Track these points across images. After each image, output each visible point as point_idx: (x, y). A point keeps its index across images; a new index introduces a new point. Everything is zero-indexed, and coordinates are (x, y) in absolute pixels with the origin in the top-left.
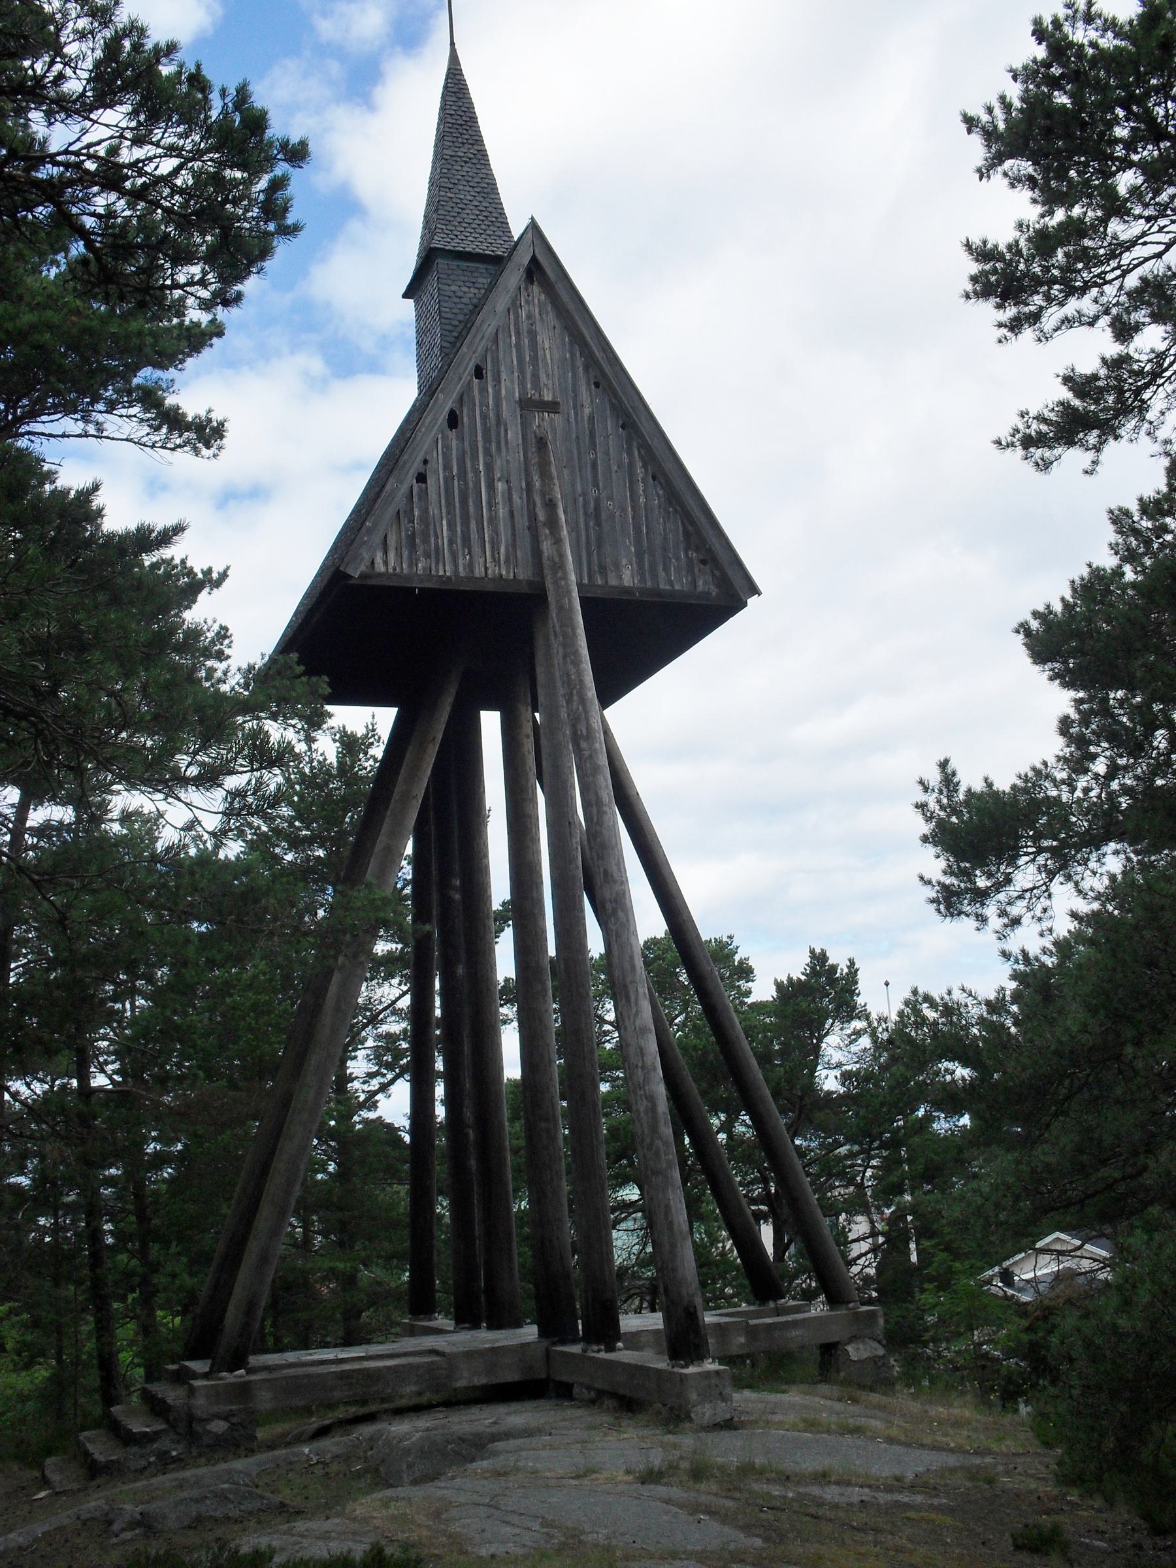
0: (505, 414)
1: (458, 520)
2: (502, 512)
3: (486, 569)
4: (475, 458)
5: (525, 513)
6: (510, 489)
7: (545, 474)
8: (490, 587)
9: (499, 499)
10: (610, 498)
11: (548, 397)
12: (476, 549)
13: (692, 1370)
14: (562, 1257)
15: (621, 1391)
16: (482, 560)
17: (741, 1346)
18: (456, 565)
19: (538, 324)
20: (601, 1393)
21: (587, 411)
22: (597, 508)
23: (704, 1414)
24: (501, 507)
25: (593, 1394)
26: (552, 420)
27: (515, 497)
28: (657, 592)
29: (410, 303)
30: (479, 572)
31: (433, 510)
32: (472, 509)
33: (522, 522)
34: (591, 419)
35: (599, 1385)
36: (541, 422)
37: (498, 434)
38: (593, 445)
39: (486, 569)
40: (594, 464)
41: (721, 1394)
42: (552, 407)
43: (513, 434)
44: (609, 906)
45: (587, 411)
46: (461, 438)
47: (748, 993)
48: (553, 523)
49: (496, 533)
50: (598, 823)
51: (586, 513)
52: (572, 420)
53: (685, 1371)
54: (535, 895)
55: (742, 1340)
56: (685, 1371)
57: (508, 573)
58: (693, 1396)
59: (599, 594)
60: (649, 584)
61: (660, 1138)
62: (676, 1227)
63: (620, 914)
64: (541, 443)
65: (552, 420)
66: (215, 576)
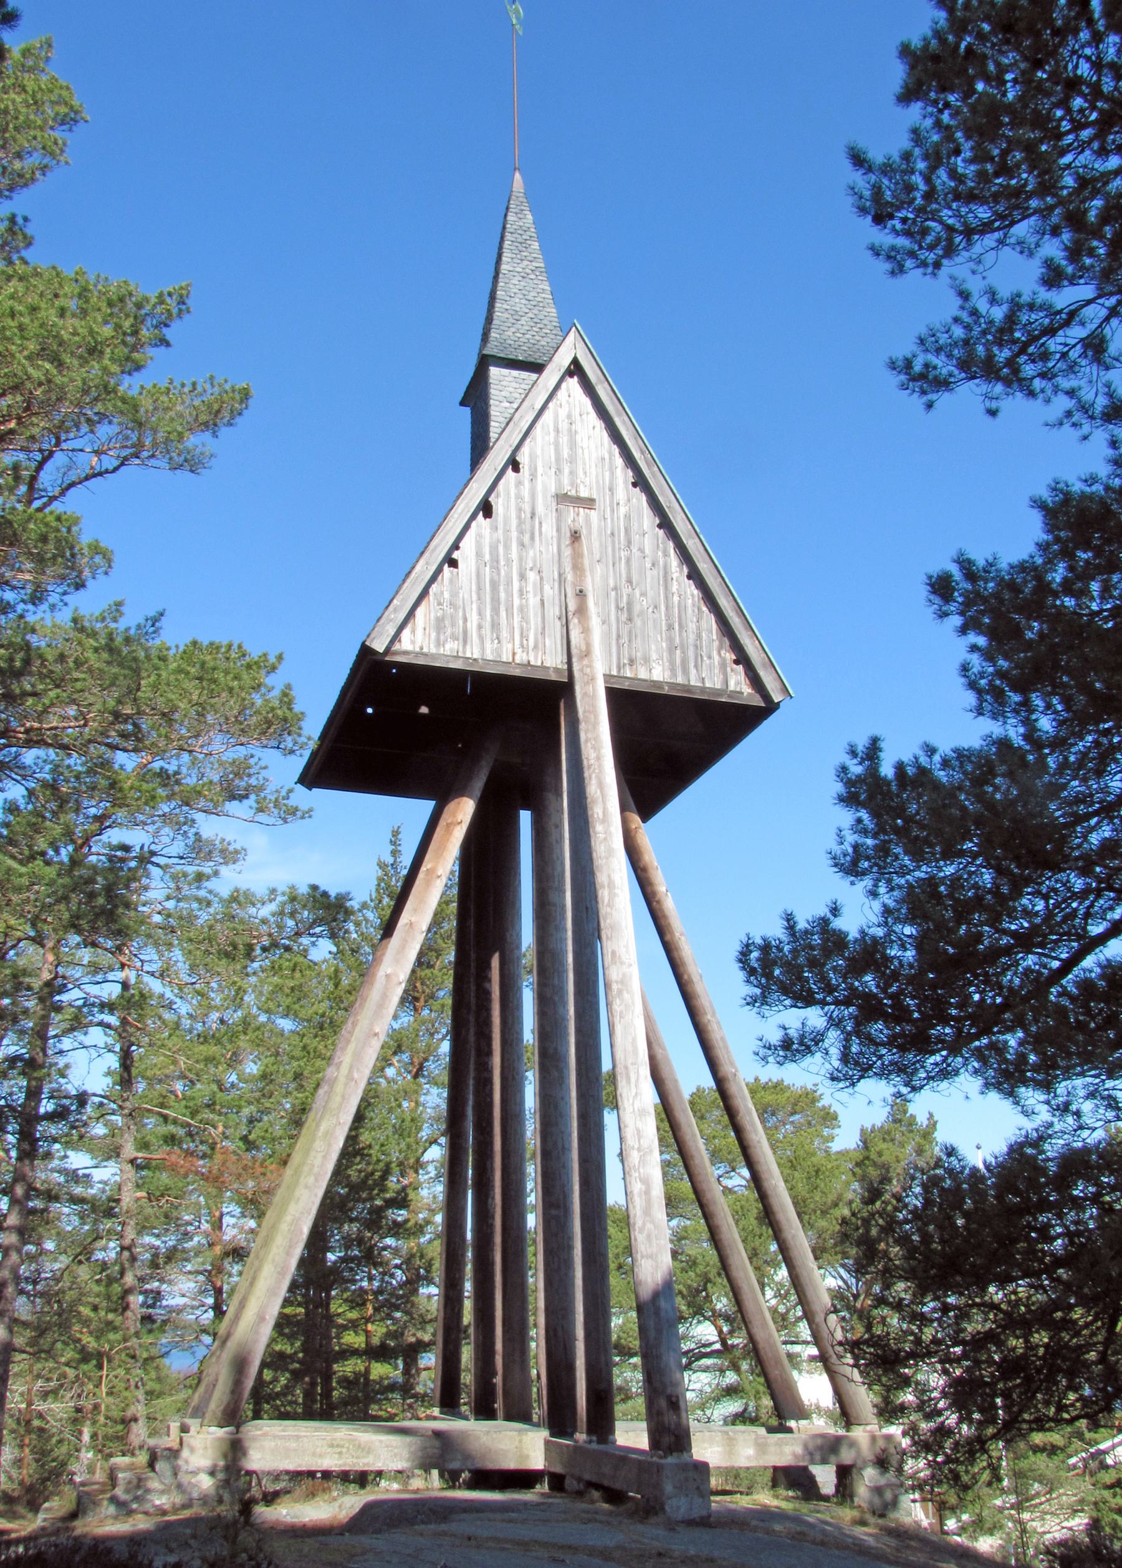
0: (540, 509)
1: (488, 607)
2: (533, 601)
3: (514, 654)
4: (507, 547)
5: (557, 601)
6: (541, 579)
7: (577, 567)
8: (517, 672)
9: (530, 588)
10: (643, 594)
11: (584, 493)
12: (504, 634)
13: (670, 1460)
14: (565, 1348)
15: (606, 1483)
16: (510, 646)
17: (749, 1458)
18: (483, 648)
19: (579, 423)
20: (591, 1485)
21: (623, 510)
22: (630, 604)
23: (679, 1508)
24: (531, 595)
25: (582, 1486)
26: (587, 516)
27: (547, 588)
28: (687, 688)
29: (467, 411)
30: (506, 657)
31: (464, 594)
32: (502, 595)
33: (553, 611)
34: (628, 517)
35: (587, 1477)
36: (574, 517)
37: (533, 527)
38: (629, 543)
39: (514, 654)
40: (628, 560)
41: (698, 1488)
42: (589, 503)
43: (549, 529)
44: (615, 987)
45: (623, 510)
46: (495, 528)
47: (832, 1138)
48: (582, 610)
49: (524, 619)
50: (609, 905)
51: (617, 607)
52: (608, 515)
53: (663, 1461)
54: (556, 981)
55: (751, 1451)
56: (663, 1461)
57: (536, 658)
58: (668, 1488)
59: (626, 686)
60: (680, 680)
61: (653, 1222)
62: (663, 1314)
63: (626, 995)
64: (575, 536)
65: (587, 516)
66: (272, 659)
